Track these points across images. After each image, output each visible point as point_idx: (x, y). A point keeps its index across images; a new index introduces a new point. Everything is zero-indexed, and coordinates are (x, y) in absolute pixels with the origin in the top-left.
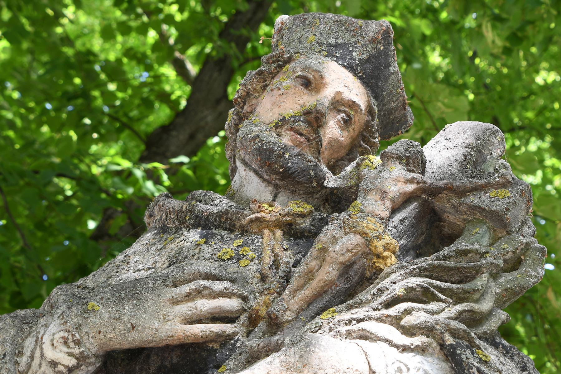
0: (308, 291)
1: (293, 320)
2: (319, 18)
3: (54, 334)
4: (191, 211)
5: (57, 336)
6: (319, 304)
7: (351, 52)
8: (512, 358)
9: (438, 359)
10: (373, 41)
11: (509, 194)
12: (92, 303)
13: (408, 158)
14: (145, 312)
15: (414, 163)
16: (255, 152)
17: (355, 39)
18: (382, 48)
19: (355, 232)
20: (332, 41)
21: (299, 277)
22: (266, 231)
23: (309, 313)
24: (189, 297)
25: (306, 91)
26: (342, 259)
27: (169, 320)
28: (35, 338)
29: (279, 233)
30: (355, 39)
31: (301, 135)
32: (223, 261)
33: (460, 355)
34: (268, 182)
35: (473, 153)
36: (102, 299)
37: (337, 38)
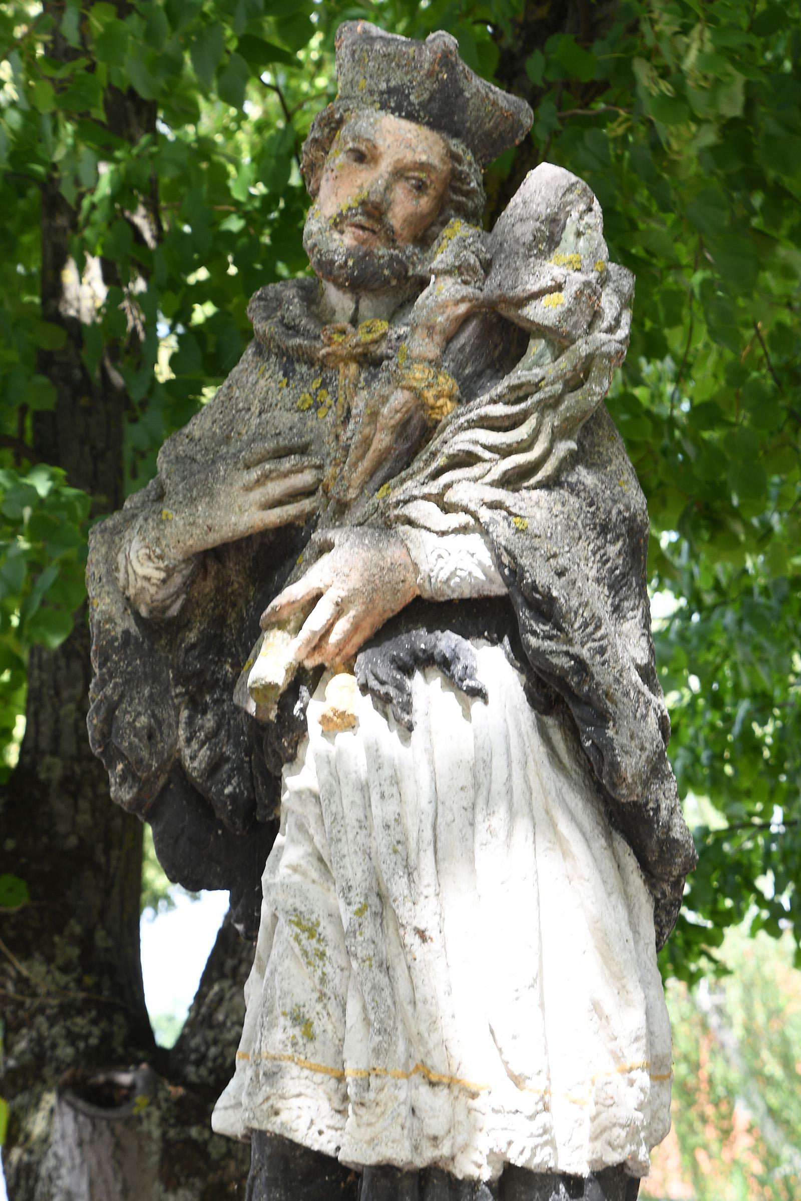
0: (365, 464)
1: (357, 496)
2: (367, 51)
3: (137, 551)
6: (381, 474)
7: (409, 94)
8: (578, 495)
10: (430, 74)
12: (165, 511)
13: (459, 267)
14: (219, 508)
15: (467, 271)
17: (409, 77)
18: (445, 76)
19: (403, 388)
20: (383, 86)
21: (356, 448)
23: (372, 485)
24: (259, 482)
25: (363, 166)
26: (393, 422)
27: (246, 511)
30: (409, 77)
32: (303, 411)
35: (543, 228)
36: (174, 504)
37: (388, 81)
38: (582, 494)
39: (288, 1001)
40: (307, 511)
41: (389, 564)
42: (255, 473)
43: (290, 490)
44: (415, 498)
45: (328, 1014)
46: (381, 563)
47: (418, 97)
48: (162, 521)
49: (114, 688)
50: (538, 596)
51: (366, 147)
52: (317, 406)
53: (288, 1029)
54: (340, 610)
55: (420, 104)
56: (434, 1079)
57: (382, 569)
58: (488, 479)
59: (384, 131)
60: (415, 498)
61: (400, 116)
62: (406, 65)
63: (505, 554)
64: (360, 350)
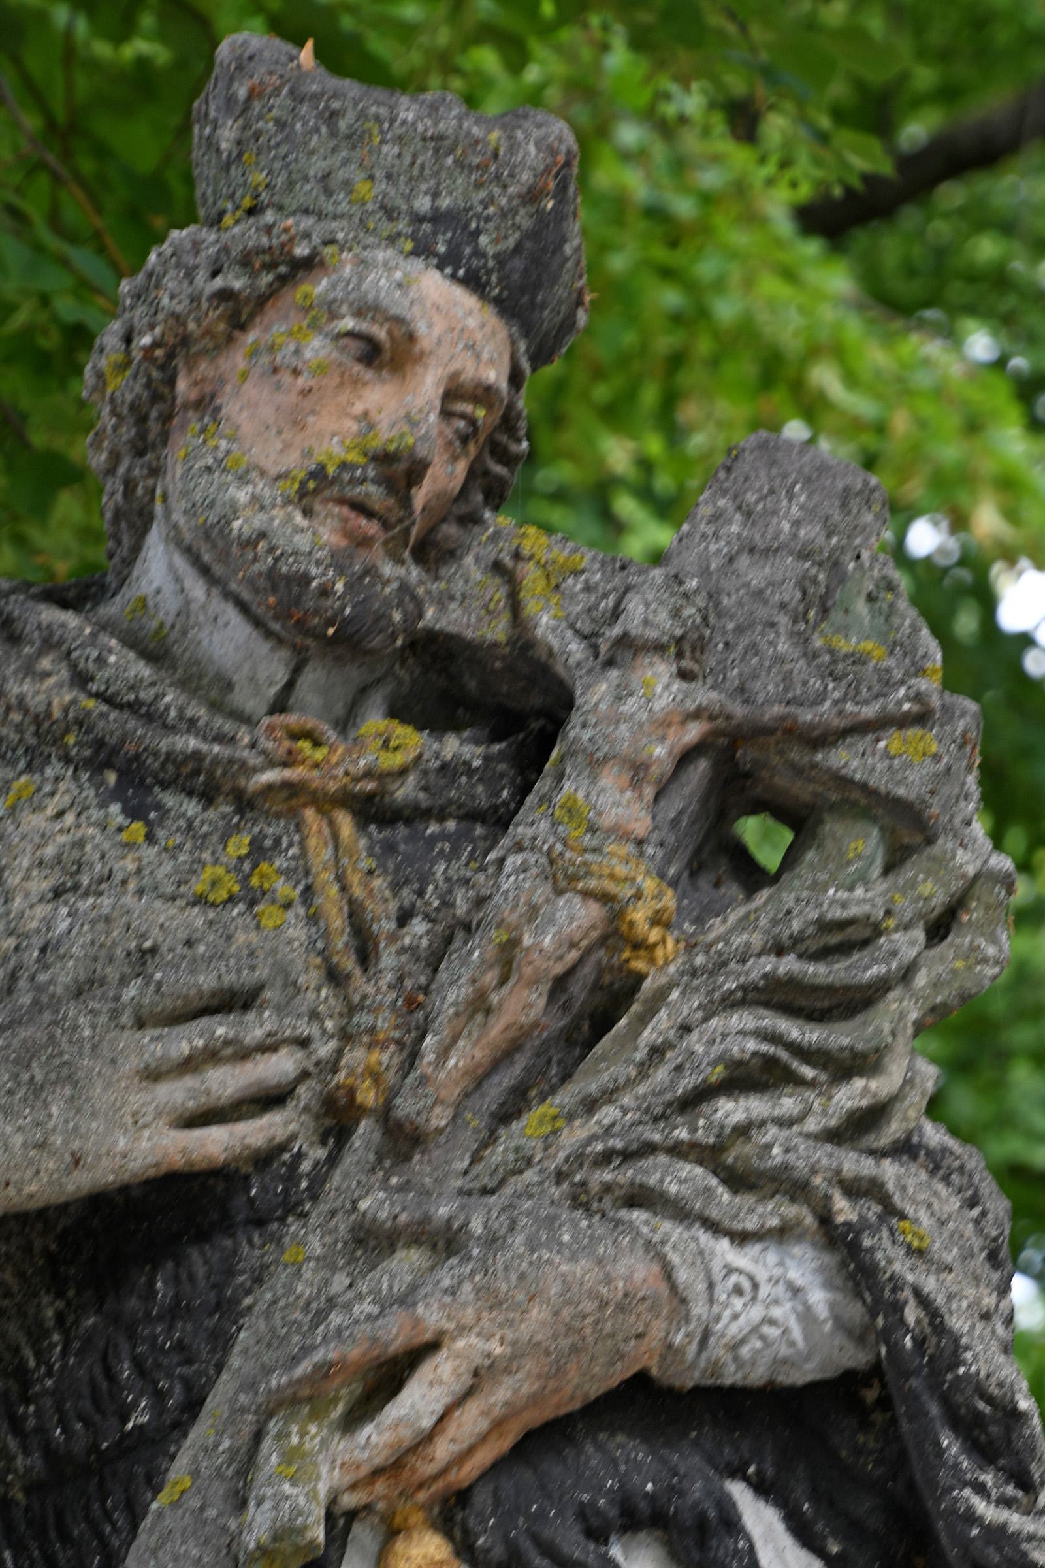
6: (507, 1079)
7: (477, 232)
8: (946, 1179)
9: (814, 1244)
10: (532, 196)
13: (679, 641)
16: (262, 582)
17: (482, 194)
18: (550, 205)
19: (586, 894)
20: (423, 204)
22: (310, 814)
24: (190, 1065)
27: (145, 1126)
30: (482, 194)
31: (369, 513)
32: (214, 905)
33: (872, 1250)
34: (280, 641)
37: (435, 195)
40: (277, 1140)
41: (620, 1294)
43: (253, 1090)
44: (650, 1148)
46: (604, 1291)
47: (496, 241)
50: (981, 1405)
51: (389, 333)
55: (496, 256)
57: (603, 1304)
58: (812, 1125)
59: (429, 305)
61: (453, 276)
62: (478, 167)
63: (912, 1302)
64: (370, 786)
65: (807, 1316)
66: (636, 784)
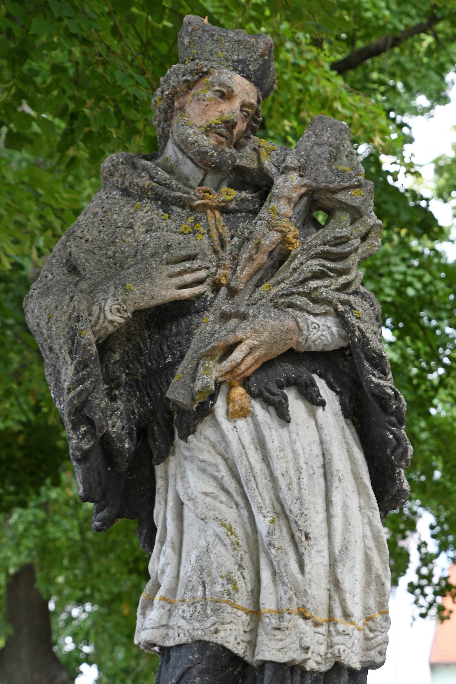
4: (152, 189)
5: (113, 307)
6: (258, 277)
7: (249, 65)
8: (366, 300)
10: (262, 55)
11: (363, 193)
13: (299, 167)
14: (156, 286)
16: (196, 153)
17: (250, 55)
19: (277, 231)
20: (235, 58)
22: (209, 211)
24: (180, 274)
28: (99, 307)
29: (218, 214)
30: (250, 55)
31: (222, 136)
33: (347, 318)
34: (201, 168)
37: (238, 55)
38: (368, 300)
39: (223, 569)
42: (178, 268)
45: (244, 577)
48: (126, 290)
49: (91, 384)
52: (195, 232)
53: (225, 586)
54: (252, 350)
56: (308, 615)
57: (282, 331)
58: (333, 287)
60: (293, 293)
61: (243, 76)
65: (332, 334)
66: (289, 203)
